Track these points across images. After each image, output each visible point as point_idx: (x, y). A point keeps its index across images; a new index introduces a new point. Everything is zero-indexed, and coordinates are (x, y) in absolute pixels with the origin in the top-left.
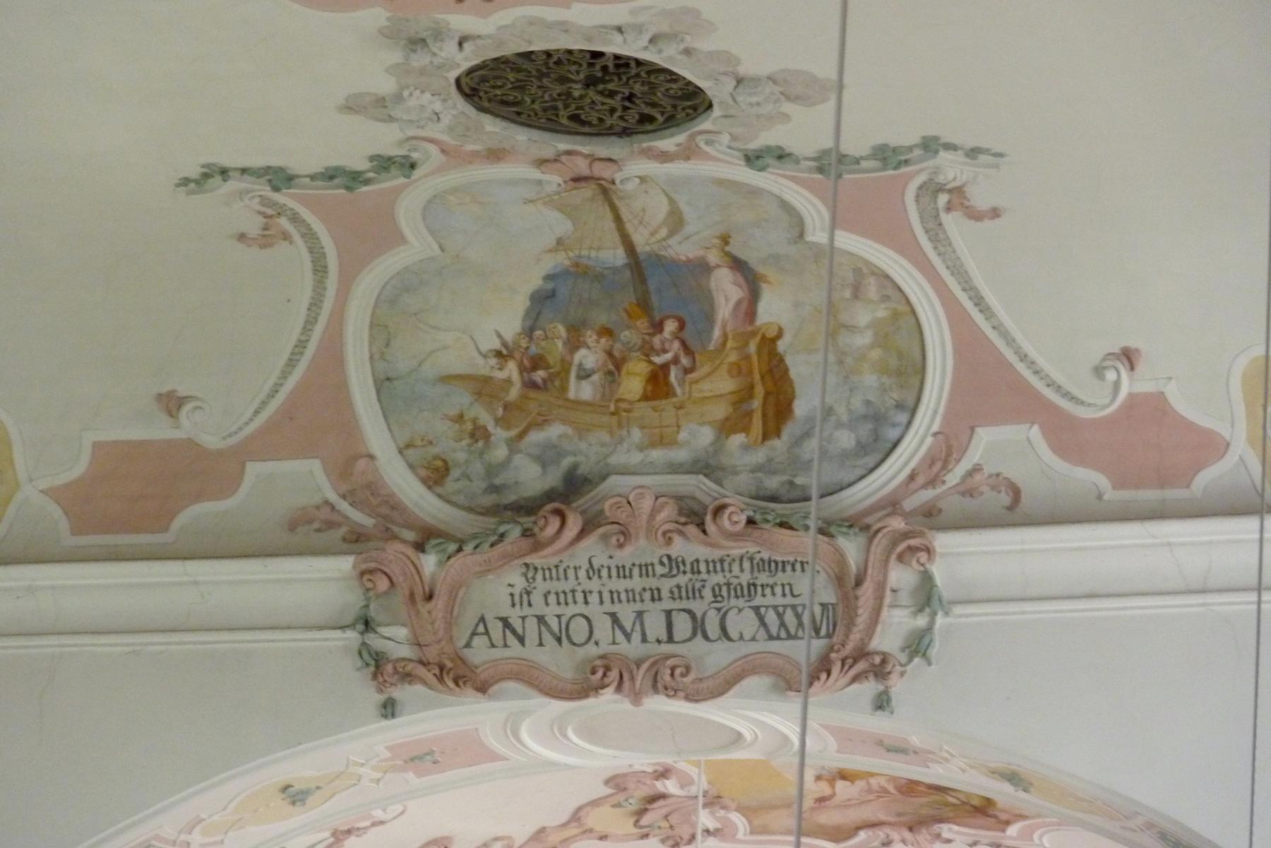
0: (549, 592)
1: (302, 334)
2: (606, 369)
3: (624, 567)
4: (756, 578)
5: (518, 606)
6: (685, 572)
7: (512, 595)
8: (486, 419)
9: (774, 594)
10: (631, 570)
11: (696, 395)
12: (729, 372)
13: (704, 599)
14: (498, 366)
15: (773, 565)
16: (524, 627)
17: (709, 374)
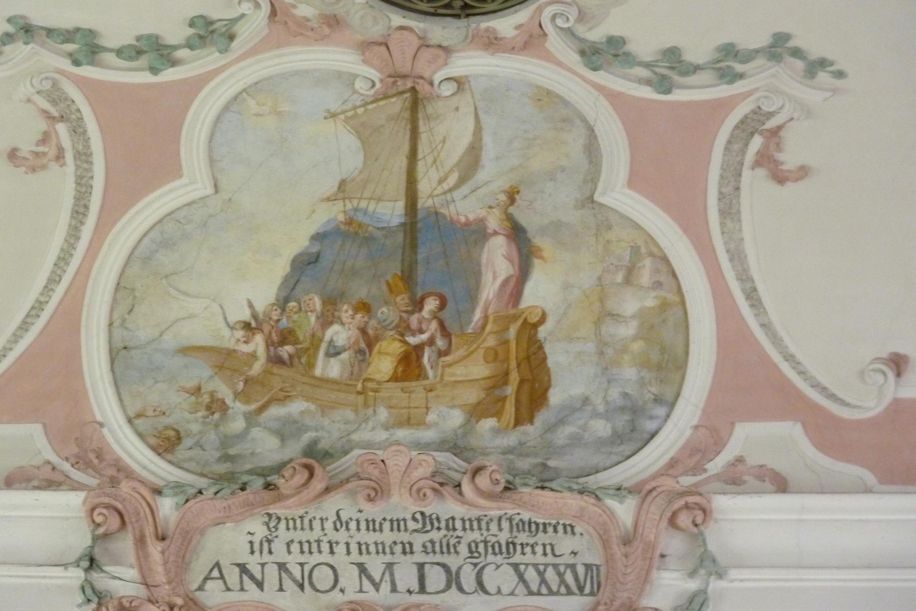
0: (292, 541)
1: (42, 294)
2: (356, 347)
3: (374, 521)
4: (516, 537)
5: (257, 554)
6: (439, 529)
7: (251, 543)
8: (225, 392)
9: (534, 553)
10: (381, 524)
11: (447, 378)
12: (485, 358)
13: (460, 554)
14: (245, 339)
15: (533, 527)
16: (263, 573)
17: (465, 358)
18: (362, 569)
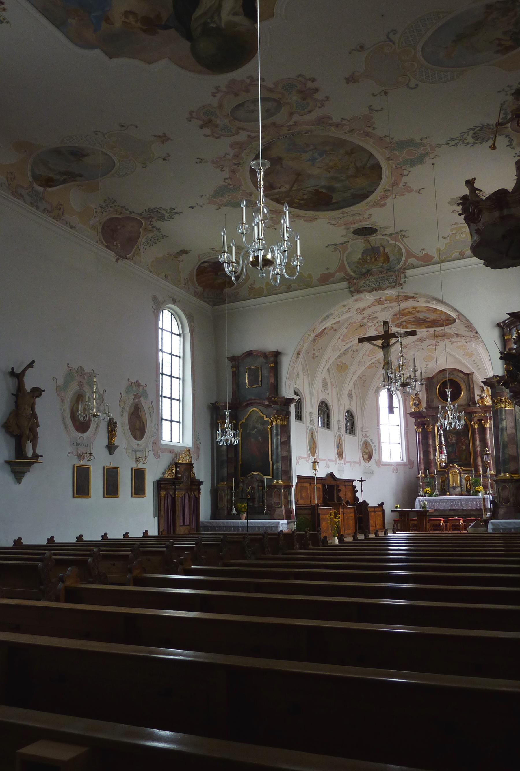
18: (374, 284)
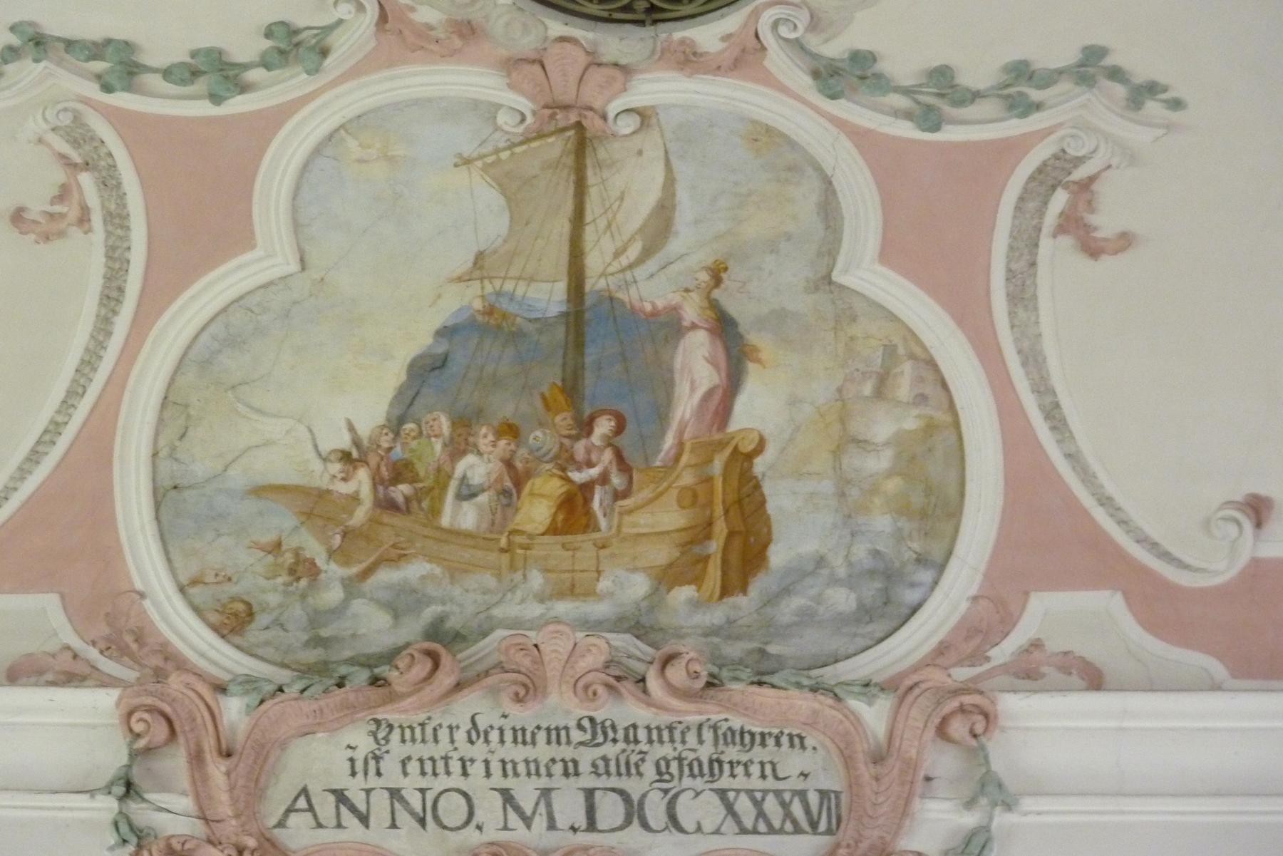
0: (409, 758)
1: (58, 412)
2: (499, 487)
3: (524, 730)
4: (722, 752)
5: (360, 776)
6: (615, 741)
7: (352, 760)
8: (315, 549)
9: (748, 774)
10: (533, 734)
11: (626, 530)
12: (679, 501)
13: (644, 777)
14: (343, 475)
15: (747, 738)
16: (368, 803)
17: (651, 501)
18: (508, 797)
